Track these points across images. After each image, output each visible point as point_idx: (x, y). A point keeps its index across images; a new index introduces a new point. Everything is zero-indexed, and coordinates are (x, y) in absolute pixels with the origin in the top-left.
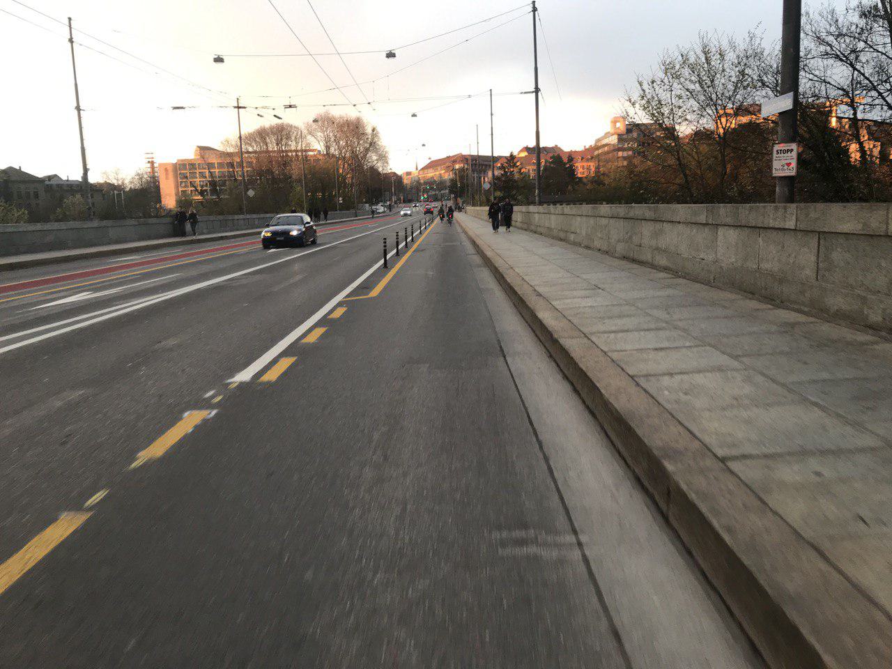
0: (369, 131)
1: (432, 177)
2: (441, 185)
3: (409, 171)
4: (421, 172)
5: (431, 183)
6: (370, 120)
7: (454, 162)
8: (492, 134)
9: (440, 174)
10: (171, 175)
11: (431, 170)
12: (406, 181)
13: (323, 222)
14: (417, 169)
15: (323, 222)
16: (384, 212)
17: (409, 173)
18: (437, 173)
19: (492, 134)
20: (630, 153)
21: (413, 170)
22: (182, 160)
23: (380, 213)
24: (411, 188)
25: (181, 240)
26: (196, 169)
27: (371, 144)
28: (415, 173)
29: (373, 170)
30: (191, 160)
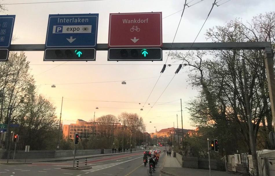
0: (139, 118)
1: (162, 136)
2: (165, 139)
3: (153, 132)
4: (158, 134)
5: (161, 138)
6: (140, 115)
7: (171, 131)
8: (182, 121)
9: (165, 135)
10: (67, 130)
11: (162, 133)
12: (152, 137)
13: (118, 153)
14: (156, 132)
15: (118, 153)
16: (143, 150)
17: (153, 134)
18: (164, 134)
19: (182, 121)
20: (241, 109)
21: (154, 132)
22: (72, 124)
23: (142, 150)
24: (154, 139)
25: (106, 166)
26: (76, 128)
27: (140, 123)
28: (155, 134)
29: (139, 132)
30: (75, 124)
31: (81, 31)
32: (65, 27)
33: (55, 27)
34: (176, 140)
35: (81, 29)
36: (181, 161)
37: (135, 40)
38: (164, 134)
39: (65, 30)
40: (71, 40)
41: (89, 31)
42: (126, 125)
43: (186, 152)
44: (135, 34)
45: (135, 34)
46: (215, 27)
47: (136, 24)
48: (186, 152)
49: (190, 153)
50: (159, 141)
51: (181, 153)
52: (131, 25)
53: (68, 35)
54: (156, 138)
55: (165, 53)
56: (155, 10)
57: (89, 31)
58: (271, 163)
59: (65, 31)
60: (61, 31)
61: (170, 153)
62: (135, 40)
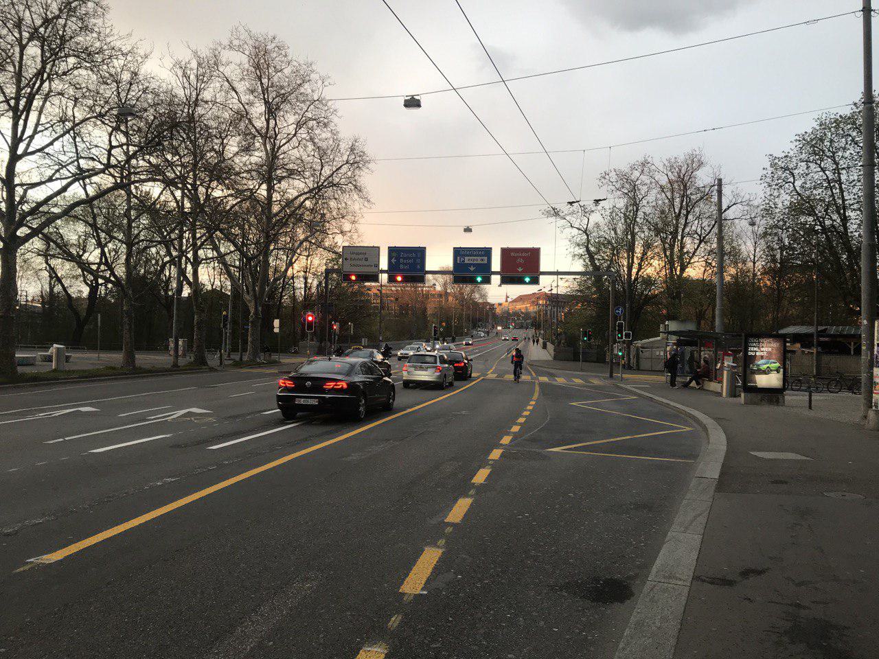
2: (527, 315)
5: (516, 314)
9: (526, 307)
12: (498, 311)
17: (500, 304)
18: (524, 306)
21: (502, 300)
29: (476, 304)
31: (479, 262)
32: (466, 258)
33: (458, 258)
34: (549, 317)
35: (478, 260)
36: (552, 352)
37: (520, 270)
38: (524, 306)
39: (467, 260)
40: (472, 269)
41: (486, 262)
42: (449, 291)
43: (559, 343)
44: (520, 265)
45: (520, 265)
46: (613, 170)
47: (520, 257)
48: (559, 343)
49: (563, 344)
50: (513, 319)
51: (553, 343)
52: (516, 258)
53: (470, 265)
54: (508, 313)
55: (542, 277)
56: (536, 246)
57: (486, 262)
58: (642, 351)
59: (466, 262)
60: (464, 261)
61: (538, 341)
62: (520, 270)
